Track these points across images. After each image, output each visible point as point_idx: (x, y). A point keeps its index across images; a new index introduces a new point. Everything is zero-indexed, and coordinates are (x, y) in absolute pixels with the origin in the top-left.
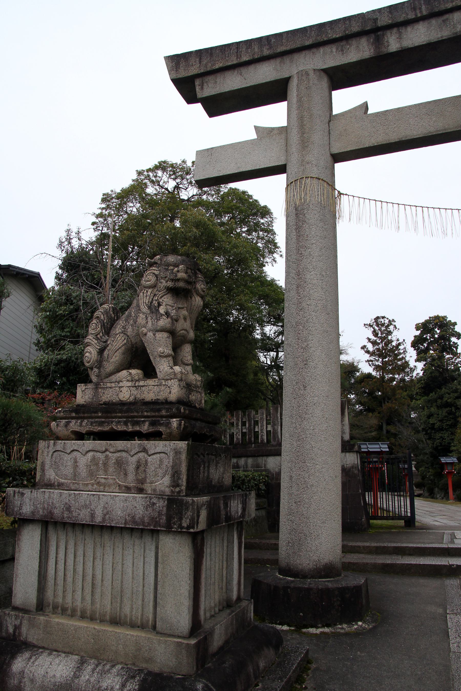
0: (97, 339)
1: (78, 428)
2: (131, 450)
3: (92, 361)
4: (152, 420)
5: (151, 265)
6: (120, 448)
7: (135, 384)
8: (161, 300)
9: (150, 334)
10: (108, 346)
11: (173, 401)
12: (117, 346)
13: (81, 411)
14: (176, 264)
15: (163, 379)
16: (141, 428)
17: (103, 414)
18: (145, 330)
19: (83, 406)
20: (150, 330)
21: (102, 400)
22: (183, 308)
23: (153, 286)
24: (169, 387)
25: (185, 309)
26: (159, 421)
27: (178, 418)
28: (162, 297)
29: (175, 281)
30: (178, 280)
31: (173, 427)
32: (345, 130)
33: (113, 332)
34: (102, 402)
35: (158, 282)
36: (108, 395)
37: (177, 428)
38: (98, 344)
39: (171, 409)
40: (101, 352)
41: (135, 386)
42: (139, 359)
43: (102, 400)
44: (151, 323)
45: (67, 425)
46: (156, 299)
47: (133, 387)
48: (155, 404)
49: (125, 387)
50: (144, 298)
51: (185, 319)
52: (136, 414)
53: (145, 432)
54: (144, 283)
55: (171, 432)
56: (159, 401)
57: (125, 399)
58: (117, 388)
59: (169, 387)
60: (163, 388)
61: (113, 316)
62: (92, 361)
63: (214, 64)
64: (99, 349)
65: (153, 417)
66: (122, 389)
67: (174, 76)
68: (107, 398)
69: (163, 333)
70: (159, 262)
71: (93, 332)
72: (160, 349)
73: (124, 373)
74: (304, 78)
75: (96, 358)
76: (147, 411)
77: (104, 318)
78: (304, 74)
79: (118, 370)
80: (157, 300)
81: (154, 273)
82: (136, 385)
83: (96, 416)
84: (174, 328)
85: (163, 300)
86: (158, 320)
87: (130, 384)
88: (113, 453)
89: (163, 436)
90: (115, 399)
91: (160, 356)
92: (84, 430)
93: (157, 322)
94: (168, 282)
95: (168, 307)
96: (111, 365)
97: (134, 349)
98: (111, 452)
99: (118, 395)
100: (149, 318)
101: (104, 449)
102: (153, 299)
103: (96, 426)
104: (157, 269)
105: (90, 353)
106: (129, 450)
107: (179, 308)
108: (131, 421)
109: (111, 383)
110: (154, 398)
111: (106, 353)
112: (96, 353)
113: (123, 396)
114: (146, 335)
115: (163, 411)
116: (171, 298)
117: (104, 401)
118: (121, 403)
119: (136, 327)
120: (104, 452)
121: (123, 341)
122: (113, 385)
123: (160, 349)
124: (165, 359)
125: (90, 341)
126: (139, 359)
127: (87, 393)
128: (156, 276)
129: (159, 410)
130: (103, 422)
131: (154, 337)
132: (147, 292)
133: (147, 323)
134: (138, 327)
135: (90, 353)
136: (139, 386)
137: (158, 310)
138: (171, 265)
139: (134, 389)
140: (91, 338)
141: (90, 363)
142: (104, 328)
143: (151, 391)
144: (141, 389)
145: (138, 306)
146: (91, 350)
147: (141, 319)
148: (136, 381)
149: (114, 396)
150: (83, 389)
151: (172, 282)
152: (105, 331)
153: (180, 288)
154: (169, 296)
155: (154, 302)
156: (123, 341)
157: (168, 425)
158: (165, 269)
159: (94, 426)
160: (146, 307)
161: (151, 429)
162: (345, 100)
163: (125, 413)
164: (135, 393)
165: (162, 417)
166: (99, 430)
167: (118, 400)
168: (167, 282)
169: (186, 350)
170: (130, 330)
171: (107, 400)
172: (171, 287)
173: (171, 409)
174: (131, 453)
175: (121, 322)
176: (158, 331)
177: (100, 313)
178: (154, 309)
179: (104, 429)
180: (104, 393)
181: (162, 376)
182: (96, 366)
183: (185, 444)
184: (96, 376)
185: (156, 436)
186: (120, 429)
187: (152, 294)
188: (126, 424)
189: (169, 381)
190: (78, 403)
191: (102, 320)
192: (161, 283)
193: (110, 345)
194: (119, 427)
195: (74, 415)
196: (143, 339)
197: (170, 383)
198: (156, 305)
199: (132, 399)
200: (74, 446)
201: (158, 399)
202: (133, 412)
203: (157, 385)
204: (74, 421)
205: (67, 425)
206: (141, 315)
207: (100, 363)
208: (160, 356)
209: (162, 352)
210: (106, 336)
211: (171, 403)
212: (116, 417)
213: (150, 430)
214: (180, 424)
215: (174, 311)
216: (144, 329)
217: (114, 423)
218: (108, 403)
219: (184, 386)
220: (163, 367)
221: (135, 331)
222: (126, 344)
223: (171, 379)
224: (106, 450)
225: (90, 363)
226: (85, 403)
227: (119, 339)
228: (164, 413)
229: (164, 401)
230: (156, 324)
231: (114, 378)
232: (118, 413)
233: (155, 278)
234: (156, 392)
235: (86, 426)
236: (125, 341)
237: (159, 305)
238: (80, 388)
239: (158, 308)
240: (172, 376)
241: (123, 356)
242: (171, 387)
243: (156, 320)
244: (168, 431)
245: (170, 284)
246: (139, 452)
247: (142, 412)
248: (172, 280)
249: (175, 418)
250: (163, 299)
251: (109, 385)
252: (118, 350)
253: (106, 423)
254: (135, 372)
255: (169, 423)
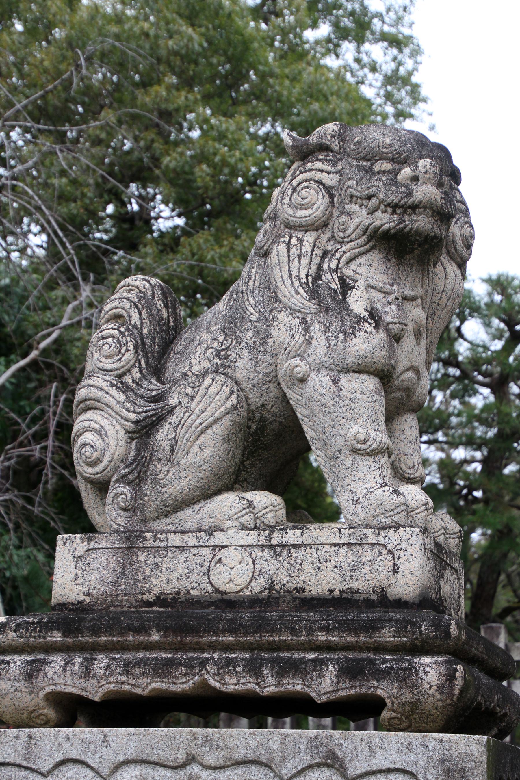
0: (125, 389)
1: (77, 682)
2: (284, 761)
3: (106, 460)
4: (347, 659)
5: (305, 154)
6: (240, 754)
7: (269, 538)
8: (348, 272)
9: (320, 381)
10: (171, 411)
11: (406, 598)
12: (208, 413)
13: (83, 626)
14: (399, 153)
15: (367, 527)
16: (309, 686)
17: (165, 636)
18: (301, 367)
19: (80, 608)
20: (320, 367)
21: (149, 591)
22: (413, 299)
23: (321, 225)
24: (390, 552)
25: (419, 301)
26: (371, 662)
27: (438, 654)
28: (351, 260)
29: (405, 212)
30: (414, 208)
31: (426, 686)
33: (174, 368)
34: (149, 597)
35: (336, 213)
36: (173, 573)
37: (440, 689)
38: (128, 405)
39: (413, 624)
40: (143, 431)
41: (271, 546)
42: (274, 456)
43: (149, 591)
44: (323, 342)
45: (31, 673)
46: (333, 265)
47: (262, 547)
48: (351, 609)
49: (231, 547)
50: (286, 265)
51: (418, 334)
52: (286, 637)
53: (324, 699)
54: (290, 211)
55: (419, 701)
56: (356, 596)
57: (231, 588)
58: (205, 551)
59: (390, 552)
60: (368, 554)
61: (165, 315)
62: (106, 460)
64: (136, 422)
65: (348, 648)
66: (222, 554)
68: (169, 581)
69: (364, 376)
70: (335, 145)
71: (109, 367)
72: (356, 429)
73: (228, 502)
75: (121, 451)
76: (327, 630)
77: (141, 319)
79: (207, 494)
80: (336, 271)
81: (320, 183)
82: (274, 542)
83: (140, 643)
84: (393, 362)
85: (355, 272)
86: (348, 335)
87: (251, 538)
88: (215, 768)
89: (385, 714)
90: (197, 586)
91: (355, 451)
92: (96, 691)
93: (344, 341)
94: (379, 214)
95: (374, 294)
96: (183, 474)
97: (254, 426)
98: (206, 767)
99: (208, 573)
100: (316, 329)
101: (182, 756)
102: (320, 267)
103: (143, 675)
104: (329, 168)
105: (101, 433)
106: (277, 759)
107: (405, 298)
108: (273, 662)
109: (183, 532)
110: (339, 587)
111: (163, 435)
112: (122, 433)
113: (225, 577)
114: (303, 380)
115: (386, 631)
116: (382, 267)
117: (156, 591)
118: (222, 600)
119: (265, 353)
120: (183, 766)
121: (227, 398)
122: (191, 540)
123: (356, 429)
124: (369, 460)
125: (99, 394)
126: (274, 456)
127: (94, 565)
128: (329, 191)
129: (371, 627)
130: (169, 663)
131: (333, 388)
132: (301, 241)
133: (309, 342)
134: (275, 356)
135: (101, 433)
136: (284, 546)
137: (343, 303)
138: (382, 157)
139: (267, 553)
140: (104, 385)
141: (100, 467)
142: (145, 354)
143: (322, 562)
144: (290, 555)
145: (268, 286)
146: (105, 423)
147: (284, 329)
148: (272, 529)
149: (193, 577)
150: (81, 549)
151: (394, 213)
152: (147, 363)
153: (418, 233)
154: (375, 257)
155: (327, 276)
156: (227, 398)
157: (407, 677)
158: (360, 168)
159: (135, 677)
160: (301, 290)
161: (347, 690)
163: (247, 634)
164: (271, 566)
165: (380, 648)
166: (155, 689)
167: (210, 589)
168: (371, 212)
169: (408, 432)
170: (243, 365)
171: (169, 589)
172: (388, 231)
173: (413, 624)
174: (284, 771)
175: (205, 336)
176: (348, 370)
177: (127, 305)
178: (330, 298)
179: (174, 688)
180: (157, 566)
181: (362, 515)
182: (124, 476)
183: (479, 743)
184: (124, 509)
185: (358, 711)
186: (231, 689)
187: (316, 251)
188: (254, 668)
189: (391, 533)
190: (62, 600)
191: (135, 326)
192: (349, 214)
193: (179, 412)
194: (228, 679)
195: (57, 637)
196: (290, 394)
197: (392, 538)
198: (333, 286)
199: (258, 586)
200: (66, 745)
201: (352, 591)
202: (278, 632)
203: (348, 545)
204: (57, 661)
205: (31, 673)
206: (282, 316)
207: (139, 468)
208: (355, 451)
209: (362, 437)
210: (153, 380)
211: (400, 604)
212: (212, 647)
213: (343, 693)
214: (451, 677)
215: (394, 307)
216: (297, 361)
217: (211, 668)
218: (174, 599)
219: (431, 551)
220: (360, 487)
221: (263, 368)
222: (235, 408)
223: (397, 527)
224: (191, 759)
225: (100, 467)
226: (88, 599)
227: (213, 390)
228: (387, 635)
229: (374, 597)
230: (341, 346)
231: (190, 517)
232: (223, 632)
233: (327, 199)
234: (345, 565)
235: (106, 676)
236: (233, 399)
237: (346, 287)
238: (68, 548)
239: (344, 296)
240: (400, 518)
241: (225, 446)
242: (397, 554)
243: (341, 336)
244: (408, 696)
245: (384, 220)
246: (310, 767)
247: (310, 632)
248: (394, 207)
249: (428, 653)
250: (353, 265)
251: (174, 540)
252: (210, 426)
253: (180, 665)
254: (265, 500)
255: (412, 670)
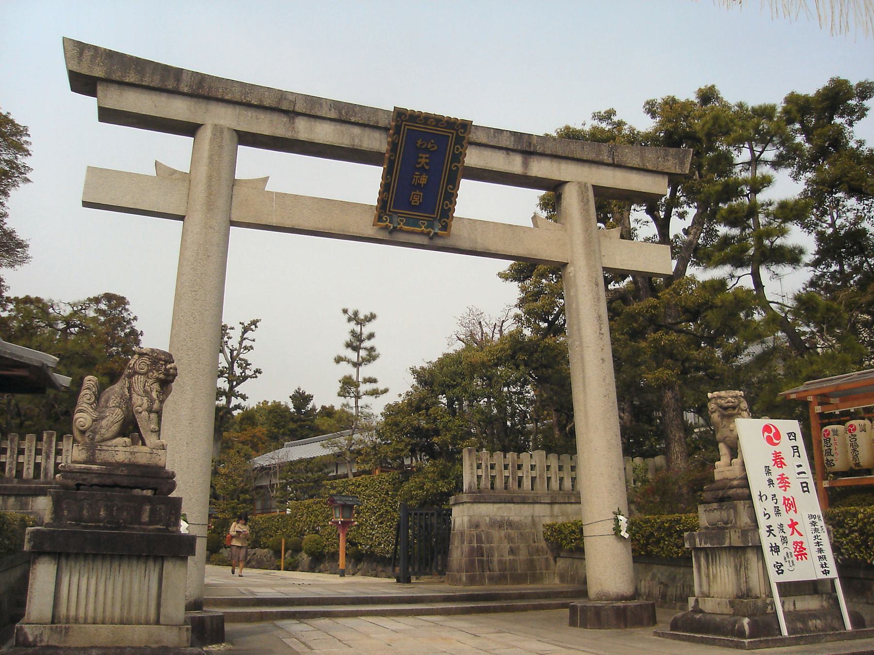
32: (246, 200)
63: (59, 372)
67: (75, 68)
74: (218, 134)
78: (218, 130)
79: (114, 437)
162: (251, 162)
